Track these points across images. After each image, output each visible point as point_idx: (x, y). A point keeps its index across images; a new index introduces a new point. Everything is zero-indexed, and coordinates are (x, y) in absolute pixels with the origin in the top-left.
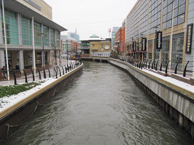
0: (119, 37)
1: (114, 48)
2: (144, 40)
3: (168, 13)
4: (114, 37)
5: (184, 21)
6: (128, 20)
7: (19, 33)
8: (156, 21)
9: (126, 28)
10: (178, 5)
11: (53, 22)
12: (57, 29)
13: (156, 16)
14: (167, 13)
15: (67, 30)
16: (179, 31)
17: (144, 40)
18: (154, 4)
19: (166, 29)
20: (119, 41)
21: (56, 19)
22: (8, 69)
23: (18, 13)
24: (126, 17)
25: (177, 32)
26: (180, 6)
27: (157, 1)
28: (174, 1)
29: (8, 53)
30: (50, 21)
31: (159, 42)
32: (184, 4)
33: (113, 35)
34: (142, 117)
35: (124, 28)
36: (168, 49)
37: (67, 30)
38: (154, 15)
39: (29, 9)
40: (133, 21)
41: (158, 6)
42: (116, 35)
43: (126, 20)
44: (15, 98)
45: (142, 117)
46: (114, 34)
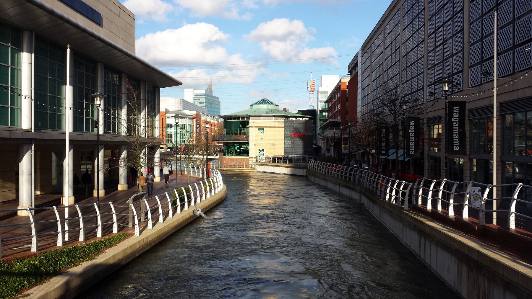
1: (323, 139)
2: (456, 109)
6: (366, 56)
9: (359, 79)
10: (512, 15)
11: (135, 59)
12: (146, 83)
13: (448, 44)
15: (180, 84)
16: (520, 91)
17: (456, 109)
18: (437, 9)
19: (482, 84)
20: (339, 119)
21: (152, 48)
23: (340, 80)
25: (515, 96)
26: (519, 18)
27: (451, 3)
28: (501, 3)
29: (69, 144)
30: (126, 54)
31: (456, 125)
37: (180, 84)
38: (442, 44)
40: (381, 59)
44: (273, 145)
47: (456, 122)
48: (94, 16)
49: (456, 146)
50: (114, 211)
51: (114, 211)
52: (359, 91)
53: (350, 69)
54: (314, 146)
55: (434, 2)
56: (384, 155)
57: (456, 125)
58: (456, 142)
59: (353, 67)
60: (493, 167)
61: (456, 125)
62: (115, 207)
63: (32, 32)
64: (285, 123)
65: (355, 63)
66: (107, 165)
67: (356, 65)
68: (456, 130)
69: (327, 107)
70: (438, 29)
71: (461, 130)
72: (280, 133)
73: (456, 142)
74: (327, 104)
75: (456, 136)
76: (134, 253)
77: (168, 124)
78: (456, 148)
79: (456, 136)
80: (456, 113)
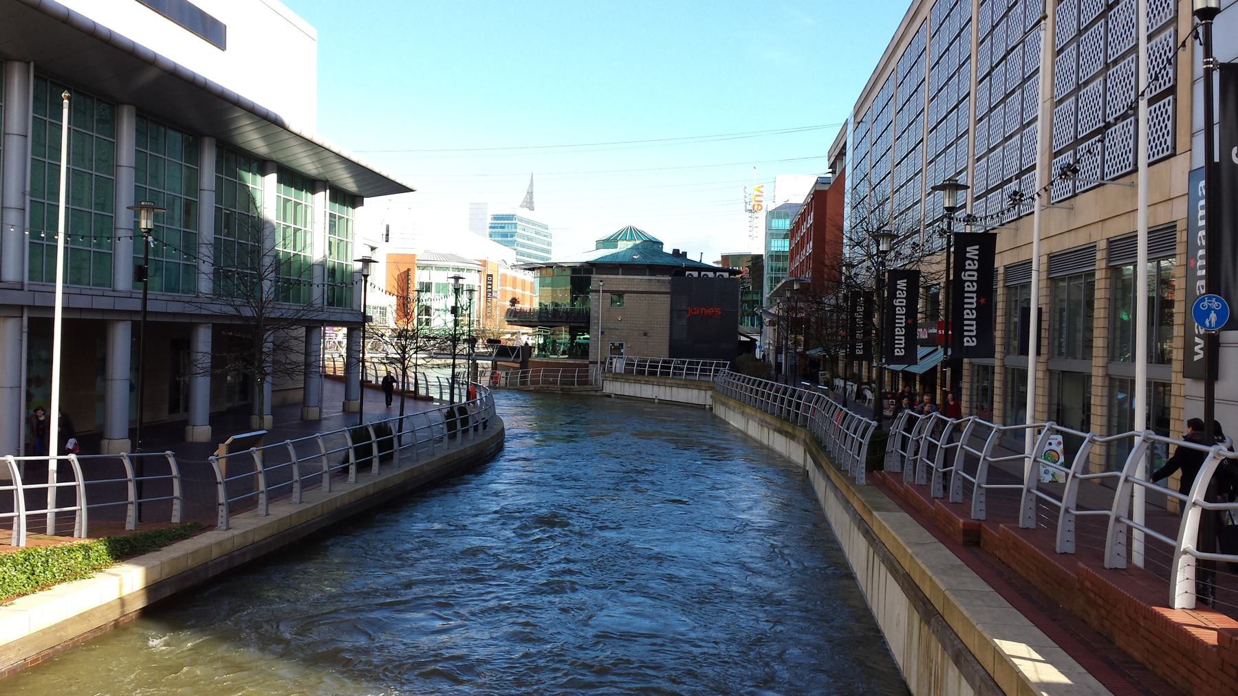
0: (809, 248)
3: (1115, 62)
4: (783, 245)
5: (1174, 148)
6: (863, 128)
7: (177, 216)
8: (1097, 84)
14: (1107, 66)
18: (1003, 25)
22: (201, 388)
24: (847, 112)
31: (971, 288)
32: (1172, 29)
33: (771, 234)
34: (1063, 679)
35: (841, 179)
36: (1025, 352)
39: (60, 425)
41: (992, 69)
42: (791, 234)
43: (851, 128)
44: (645, 334)
45: (1063, 679)
46: (785, 224)
47: (972, 282)
48: (210, 30)
49: (971, 337)
50: (175, 472)
51: (175, 472)
52: (847, 210)
53: (832, 159)
54: (743, 338)
55: (988, 3)
56: (899, 360)
57: (971, 288)
58: (971, 328)
59: (838, 155)
60: (1148, 397)
61: (972, 289)
62: (179, 464)
63: (28, 63)
64: (671, 282)
65: (841, 145)
66: (748, 410)
67: (842, 154)
68: (971, 301)
69: (787, 249)
70: (997, 65)
71: (983, 301)
72: (663, 304)
73: (971, 328)
74: (787, 242)
75: (970, 315)
76: (205, 566)
77: (422, 284)
78: (970, 342)
79: (970, 315)
80: (973, 260)
